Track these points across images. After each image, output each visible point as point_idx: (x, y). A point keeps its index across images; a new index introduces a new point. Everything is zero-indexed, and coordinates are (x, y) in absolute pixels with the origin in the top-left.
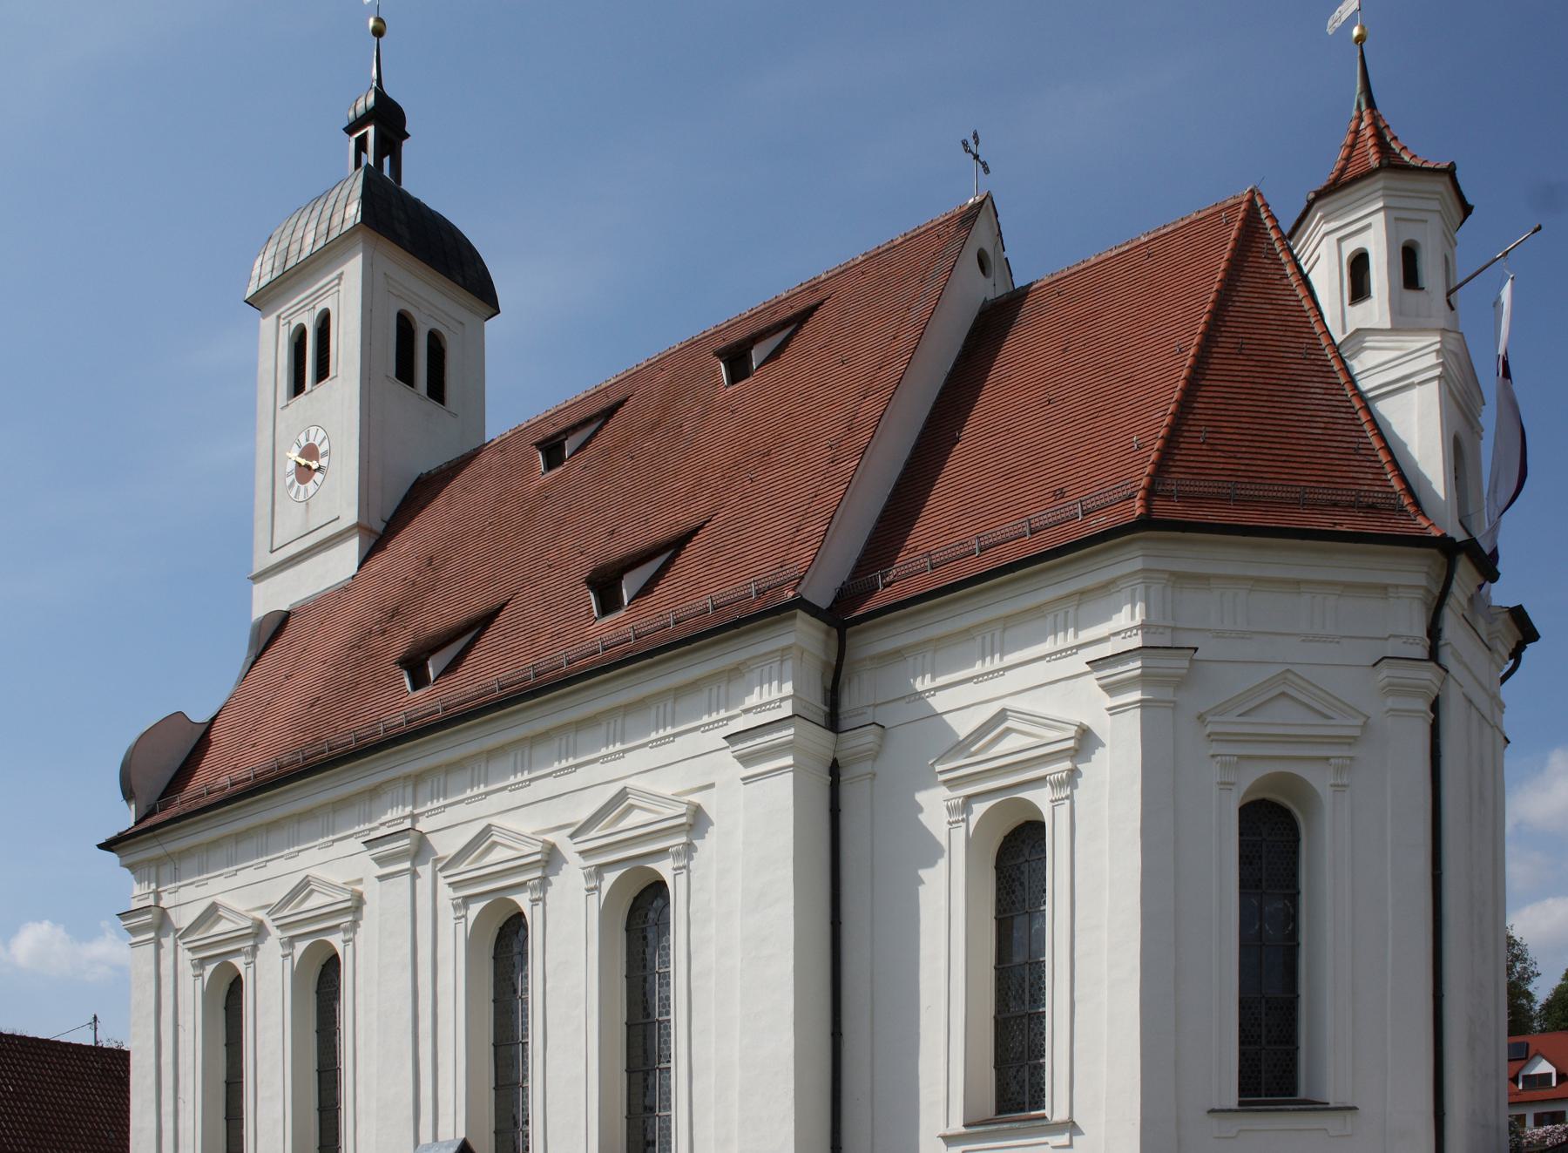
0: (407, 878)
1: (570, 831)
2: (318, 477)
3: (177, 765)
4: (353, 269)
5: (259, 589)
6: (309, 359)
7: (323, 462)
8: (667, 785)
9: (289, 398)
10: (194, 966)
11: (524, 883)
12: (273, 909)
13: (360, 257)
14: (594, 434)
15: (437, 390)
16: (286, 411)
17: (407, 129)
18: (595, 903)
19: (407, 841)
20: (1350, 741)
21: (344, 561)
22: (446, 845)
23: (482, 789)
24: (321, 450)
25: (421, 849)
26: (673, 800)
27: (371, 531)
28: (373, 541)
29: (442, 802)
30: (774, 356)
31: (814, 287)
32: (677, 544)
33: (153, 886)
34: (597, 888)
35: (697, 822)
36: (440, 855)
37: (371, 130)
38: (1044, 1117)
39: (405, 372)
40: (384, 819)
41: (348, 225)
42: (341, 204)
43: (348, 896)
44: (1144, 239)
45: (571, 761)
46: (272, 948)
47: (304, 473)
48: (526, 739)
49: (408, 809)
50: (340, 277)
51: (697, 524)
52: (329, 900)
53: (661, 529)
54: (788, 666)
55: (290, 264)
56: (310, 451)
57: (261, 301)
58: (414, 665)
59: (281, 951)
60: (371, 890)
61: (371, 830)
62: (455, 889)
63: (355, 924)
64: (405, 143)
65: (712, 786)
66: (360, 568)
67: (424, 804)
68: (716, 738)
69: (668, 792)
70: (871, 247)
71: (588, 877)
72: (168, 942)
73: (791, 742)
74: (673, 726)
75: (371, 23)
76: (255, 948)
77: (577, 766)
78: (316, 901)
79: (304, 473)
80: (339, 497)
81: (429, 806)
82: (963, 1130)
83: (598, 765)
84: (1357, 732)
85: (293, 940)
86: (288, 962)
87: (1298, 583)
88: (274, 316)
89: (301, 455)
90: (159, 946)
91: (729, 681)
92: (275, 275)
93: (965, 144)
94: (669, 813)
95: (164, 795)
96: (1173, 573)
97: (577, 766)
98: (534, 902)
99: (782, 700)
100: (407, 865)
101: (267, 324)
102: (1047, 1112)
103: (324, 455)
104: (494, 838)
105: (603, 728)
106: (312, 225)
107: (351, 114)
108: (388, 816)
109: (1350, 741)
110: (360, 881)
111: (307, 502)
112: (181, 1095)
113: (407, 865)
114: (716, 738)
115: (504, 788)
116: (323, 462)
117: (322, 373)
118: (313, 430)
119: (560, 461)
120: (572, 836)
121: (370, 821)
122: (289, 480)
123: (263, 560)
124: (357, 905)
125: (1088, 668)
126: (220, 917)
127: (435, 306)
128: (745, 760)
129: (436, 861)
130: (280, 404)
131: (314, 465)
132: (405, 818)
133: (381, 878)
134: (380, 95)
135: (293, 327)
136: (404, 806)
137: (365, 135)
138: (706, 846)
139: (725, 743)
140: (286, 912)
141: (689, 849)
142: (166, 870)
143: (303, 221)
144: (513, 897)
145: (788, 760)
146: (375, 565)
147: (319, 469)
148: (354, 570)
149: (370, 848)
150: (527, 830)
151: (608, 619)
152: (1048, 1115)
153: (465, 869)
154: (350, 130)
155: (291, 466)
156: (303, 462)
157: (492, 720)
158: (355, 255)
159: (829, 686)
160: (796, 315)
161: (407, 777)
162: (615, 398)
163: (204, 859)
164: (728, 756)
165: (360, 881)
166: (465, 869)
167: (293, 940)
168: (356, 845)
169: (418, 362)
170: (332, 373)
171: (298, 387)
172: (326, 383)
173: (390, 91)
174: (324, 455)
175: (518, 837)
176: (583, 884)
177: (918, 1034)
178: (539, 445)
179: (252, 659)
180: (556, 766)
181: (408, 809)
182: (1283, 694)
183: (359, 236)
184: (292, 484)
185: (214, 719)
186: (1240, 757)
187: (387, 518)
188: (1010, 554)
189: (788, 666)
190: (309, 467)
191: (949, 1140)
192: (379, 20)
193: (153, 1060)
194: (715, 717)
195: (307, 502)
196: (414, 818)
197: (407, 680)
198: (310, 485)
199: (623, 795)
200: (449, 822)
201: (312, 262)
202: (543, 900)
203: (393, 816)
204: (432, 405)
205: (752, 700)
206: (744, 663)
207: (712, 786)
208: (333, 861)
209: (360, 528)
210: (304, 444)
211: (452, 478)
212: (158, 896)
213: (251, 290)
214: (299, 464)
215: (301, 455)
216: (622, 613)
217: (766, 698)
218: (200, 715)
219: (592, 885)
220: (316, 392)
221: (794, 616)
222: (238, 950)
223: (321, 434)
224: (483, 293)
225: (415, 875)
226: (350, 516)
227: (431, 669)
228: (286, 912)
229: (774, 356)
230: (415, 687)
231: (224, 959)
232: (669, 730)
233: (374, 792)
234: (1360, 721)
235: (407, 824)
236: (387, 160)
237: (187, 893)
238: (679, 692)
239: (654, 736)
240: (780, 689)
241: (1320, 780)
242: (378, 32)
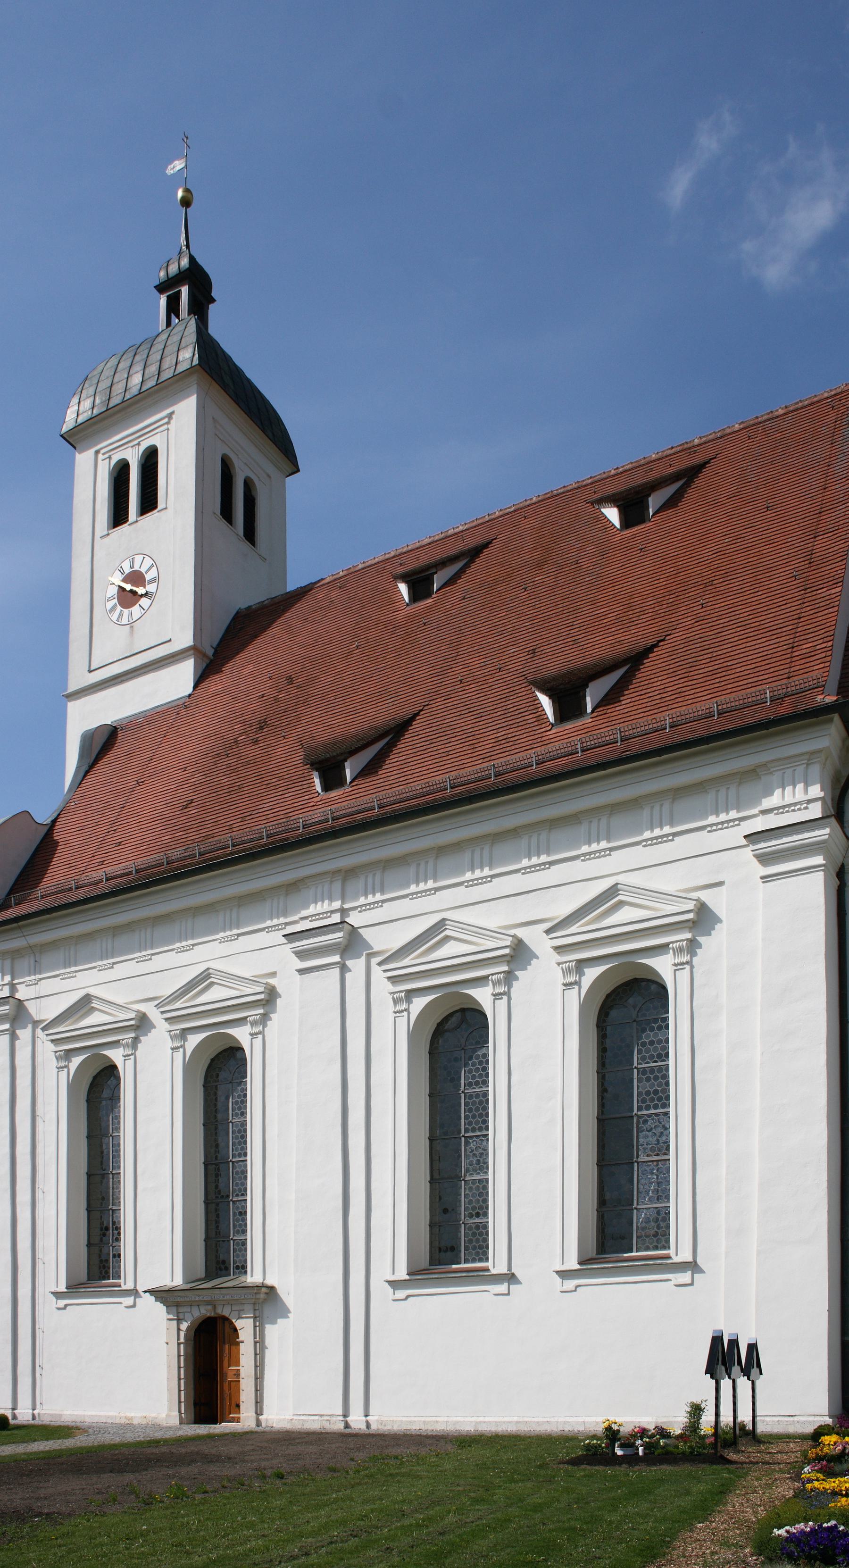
0: (336, 971)
2: (144, 602)
3: (24, 863)
4: (185, 412)
5: (73, 707)
6: (134, 492)
7: (151, 588)
8: (668, 881)
9: (137, 517)
10: (58, 1059)
11: (486, 978)
12: (162, 1003)
13: (195, 396)
14: (462, 571)
15: (250, 534)
16: (107, 539)
17: (214, 294)
18: (574, 998)
19: (340, 934)
21: (179, 681)
22: (385, 940)
23: (430, 884)
24: (148, 577)
25: (352, 943)
26: (253, 981)
27: (204, 655)
28: (205, 665)
29: (378, 897)
30: (452, 581)
32: (399, 730)
33: (8, 979)
34: (578, 983)
35: (702, 919)
36: (376, 949)
37: (185, 291)
38: (488, 1270)
39: (227, 512)
40: (304, 913)
41: (181, 368)
42: (172, 348)
43: (262, 989)
45: (544, 858)
46: (159, 1039)
47: (128, 598)
48: (148, 919)
49: (337, 904)
50: (170, 416)
51: (650, 642)
52: (236, 993)
53: (381, 714)
54: (815, 770)
55: (115, 401)
56: (136, 577)
57: (76, 438)
58: (568, 697)
59: (170, 1044)
60: (289, 984)
61: (287, 924)
62: (393, 983)
63: (265, 1018)
64: (211, 306)
65: (720, 884)
66: (195, 687)
67: (356, 898)
68: (736, 835)
69: (120, 1001)
70: (749, 417)
71: (567, 972)
72: (25, 1034)
73: (824, 842)
74: (672, 825)
75: (180, 194)
76: (136, 1040)
77: (552, 863)
78: (216, 994)
79: (128, 598)
80: (173, 617)
81: (362, 900)
82: (578, 1267)
83: (578, 862)
85: (184, 1033)
86: (179, 1055)
88: (92, 452)
89: (124, 580)
90: (14, 1037)
91: (740, 784)
92: (96, 412)
94: (123, 1016)
95: (12, 890)
97: (552, 863)
98: (497, 996)
99: (809, 801)
100: (336, 958)
101: (84, 460)
102: (489, 1264)
103: (152, 581)
104: (447, 933)
105: (646, 813)
106: (138, 367)
107: (162, 274)
108: (312, 910)
110: (273, 974)
111: (131, 625)
112: (39, 1183)
113: (336, 958)
114: (736, 835)
115: (172, 950)
116: (151, 588)
117: (149, 503)
118: (138, 559)
119: (428, 594)
120: (548, 932)
121: (285, 915)
122: (109, 605)
123: (78, 678)
124: (270, 997)
126: (93, 1009)
127: (252, 459)
128: (764, 859)
129: (370, 956)
130: (98, 534)
131: (141, 591)
132: (332, 912)
133: (302, 971)
134: (192, 259)
135: (143, 447)
136: (331, 900)
137: (178, 294)
138: (711, 944)
139: (284, 940)
140: (178, 1005)
141: (693, 946)
142: (25, 963)
143: (124, 365)
145: (819, 860)
146: (215, 684)
147: (146, 594)
148: (189, 689)
149: (290, 942)
150: (492, 923)
151: (569, 725)
152: (491, 1268)
153: (577, 932)
154: (161, 288)
155: (113, 591)
156: (128, 587)
157: (386, 832)
158: (192, 395)
160: (469, 551)
161: (337, 872)
162: (697, 460)
163: (72, 951)
164: (748, 853)
165: (273, 974)
166: (577, 932)
167: (184, 1033)
168: (277, 937)
169: (235, 505)
170: (161, 504)
171: (119, 516)
172: (151, 517)
174: (152, 581)
175: (481, 931)
176: (559, 978)
177: (828, 1153)
179: (85, 768)
180: (525, 862)
181: (337, 904)
183: (194, 378)
184: (113, 609)
185: (54, 821)
187: (215, 644)
189: (815, 770)
190: (134, 593)
191: (395, 1284)
192: (187, 190)
193: (7, 1150)
194: (723, 817)
195: (131, 625)
196: (343, 912)
197: (317, 782)
198: (136, 610)
199: (441, 925)
200: (391, 917)
201: (157, 391)
202: (508, 994)
203: (319, 910)
205: (774, 800)
206: (765, 765)
207: (720, 884)
208: (240, 954)
209: (195, 650)
210: (127, 570)
211: (285, 611)
212: (13, 987)
213: (65, 429)
214: (122, 589)
215: (124, 580)
216: (587, 720)
217: (789, 799)
218: (43, 817)
219: (572, 979)
220: (140, 529)
223: (148, 562)
224: (289, 460)
225: (344, 969)
226: (185, 638)
227: (588, 699)
228: (178, 1005)
229: (452, 581)
230: (326, 788)
231: (95, 1051)
232: (667, 830)
233: (293, 887)
235: (336, 918)
237: (48, 986)
238: (441, 851)
239: (647, 834)
240: (806, 791)
242: (186, 203)
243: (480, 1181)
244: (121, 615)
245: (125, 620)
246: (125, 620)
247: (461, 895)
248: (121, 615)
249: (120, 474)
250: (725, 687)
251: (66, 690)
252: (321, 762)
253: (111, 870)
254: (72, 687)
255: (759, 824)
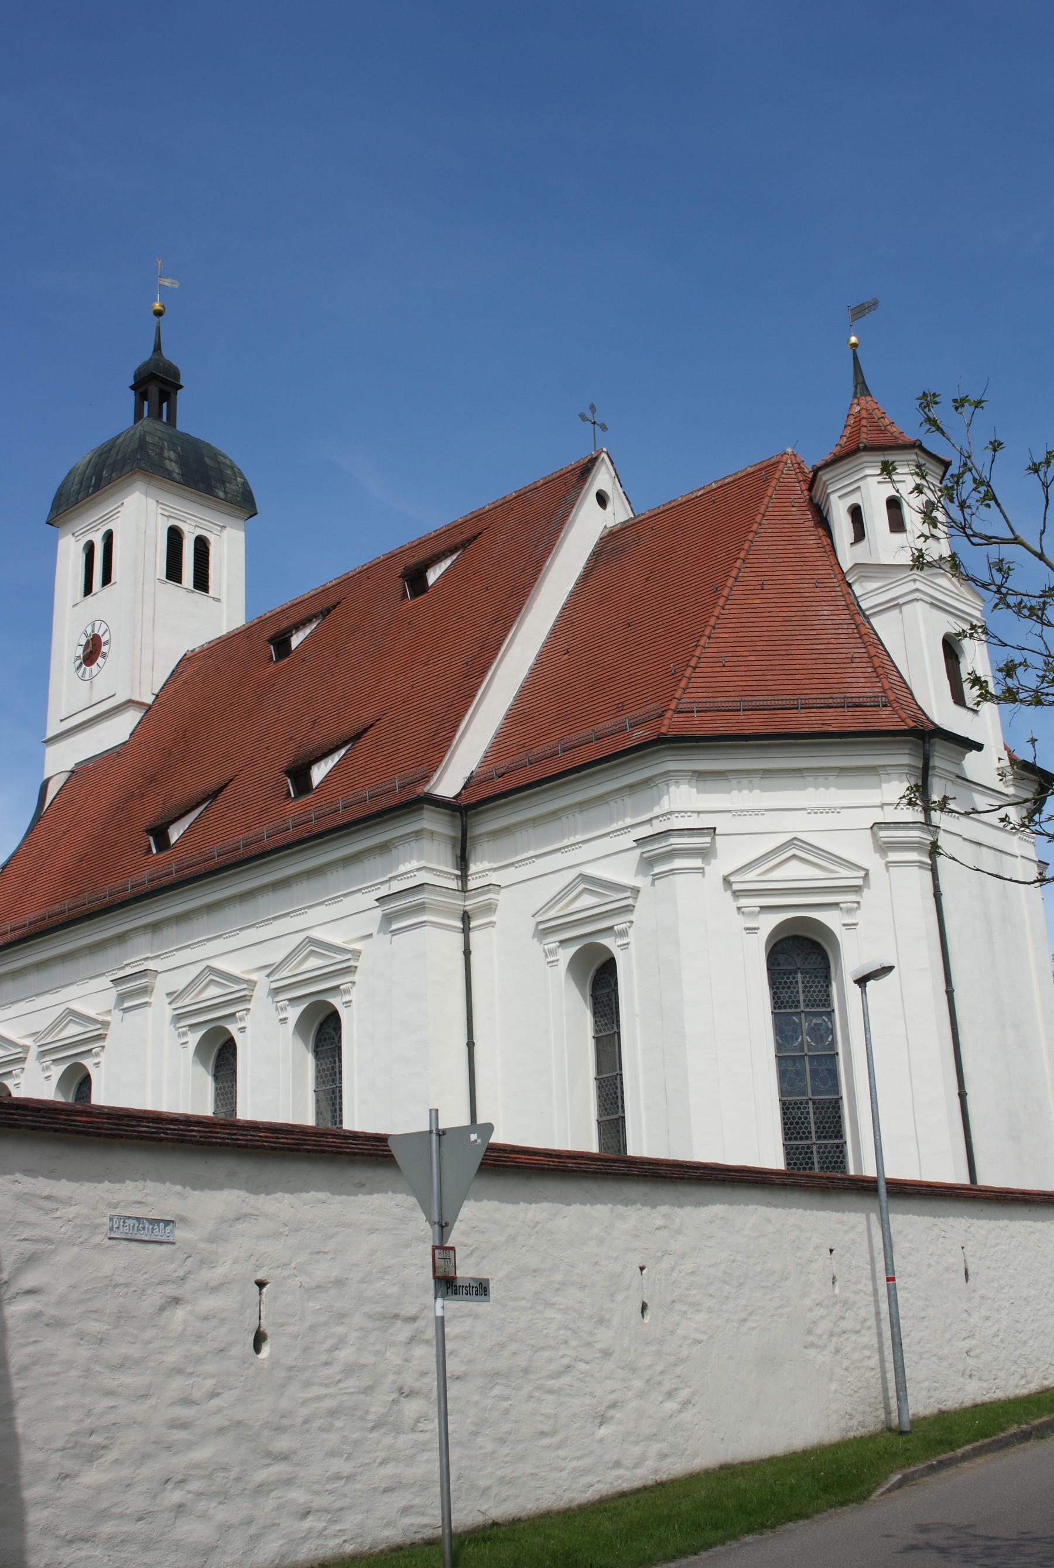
1: (268, 971)
5: (51, 751)
20: (857, 889)
31: (478, 517)
39: (174, 573)
44: (714, 486)
52: (81, 1029)
84: (860, 882)
87: (800, 770)
93: (583, 417)
96: (695, 772)
109: (857, 889)
114: (369, 899)
117: (107, 579)
118: (98, 624)
125: (635, 844)
139: (111, 985)
144: (329, 1000)
149: (116, 986)
159: (459, 854)
170: (113, 581)
171: (88, 590)
172: (108, 587)
173: (167, 354)
178: (271, 640)
182: (794, 856)
186: (762, 907)
187: (156, 691)
188: (581, 756)
204: (199, 595)
206: (389, 841)
221: (422, 808)
222: (835, 905)
223: (104, 627)
230: (160, 849)
234: (862, 873)
236: (165, 405)
241: (829, 919)
243: (790, 1139)
244: (84, 672)
245: (87, 677)
246: (87, 677)
247: (219, 945)
248: (84, 672)
249: (90, 548)
250: (737, 669)
251: (45, 736)
252: (152, 830)
253: (19, 921)
254: (50, 734)
255: (384, 891)
